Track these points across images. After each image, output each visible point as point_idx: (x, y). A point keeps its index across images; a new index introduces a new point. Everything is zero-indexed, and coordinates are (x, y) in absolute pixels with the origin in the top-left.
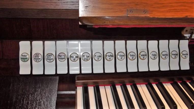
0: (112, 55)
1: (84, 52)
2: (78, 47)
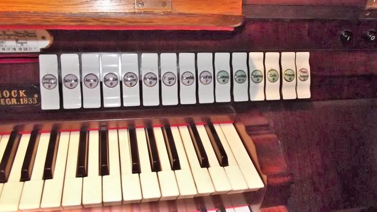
0: (209, 75)
2: (118, 63)
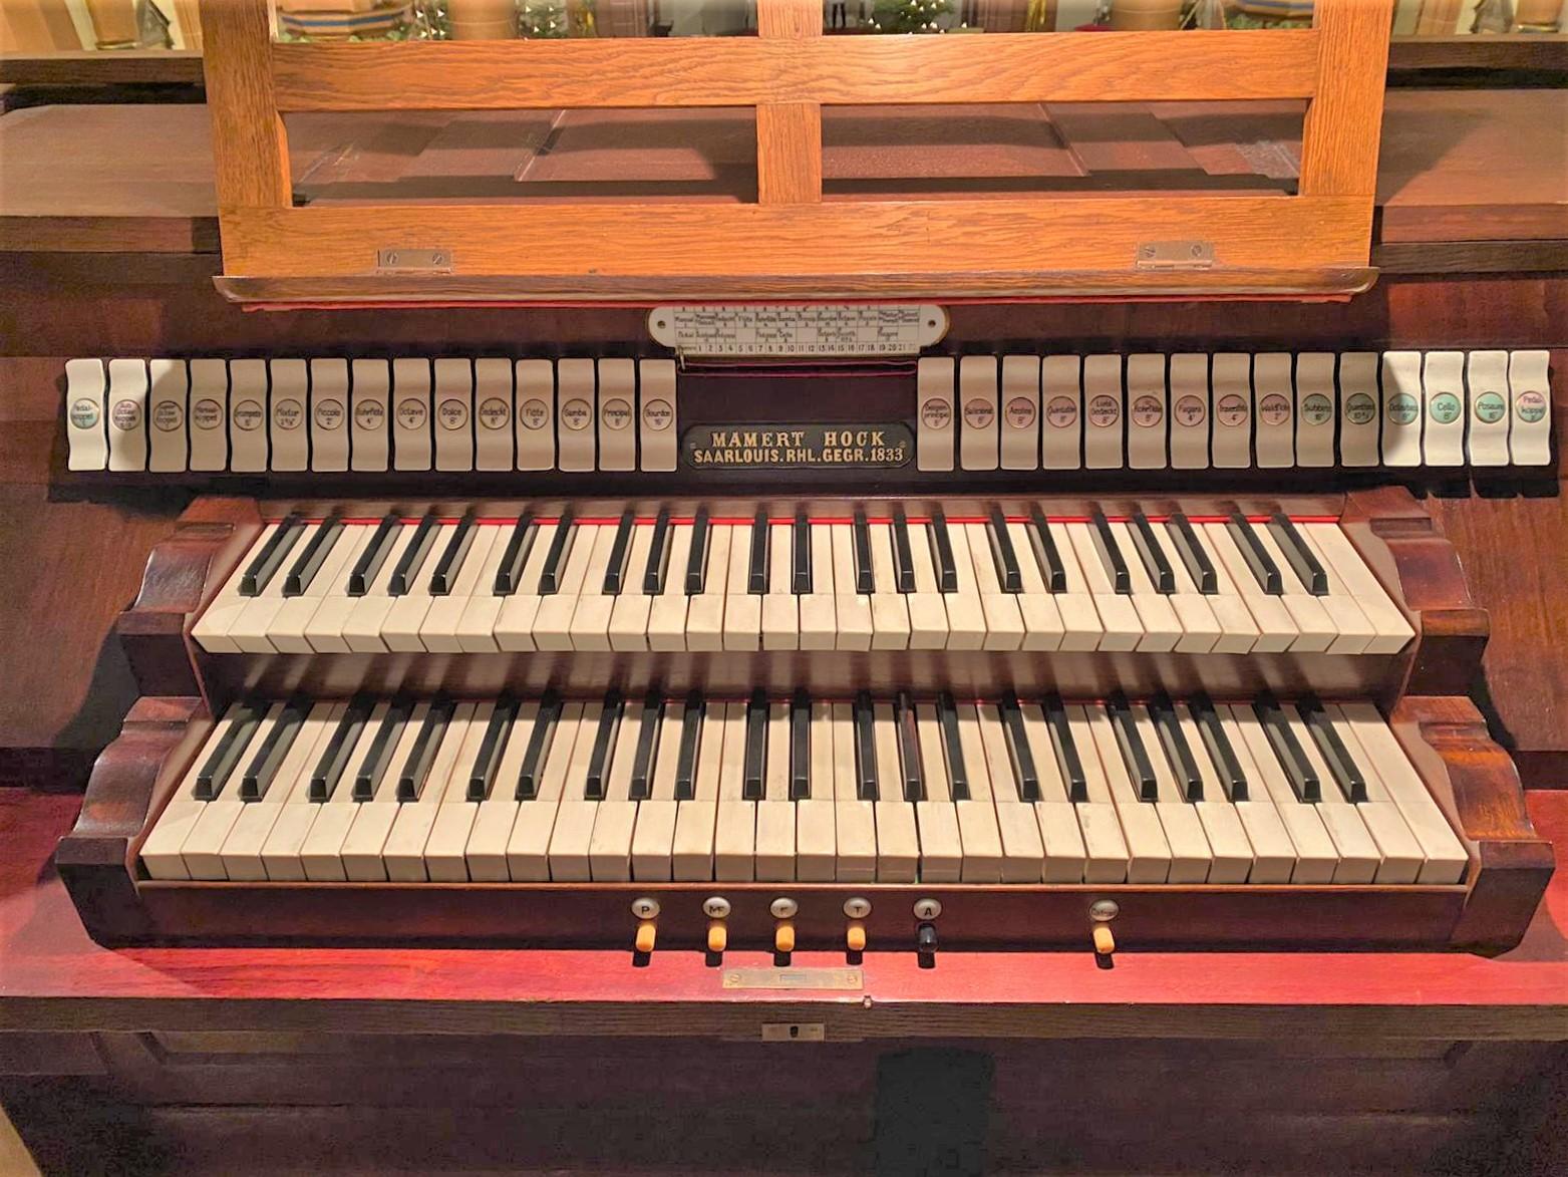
0: (1283, 403)
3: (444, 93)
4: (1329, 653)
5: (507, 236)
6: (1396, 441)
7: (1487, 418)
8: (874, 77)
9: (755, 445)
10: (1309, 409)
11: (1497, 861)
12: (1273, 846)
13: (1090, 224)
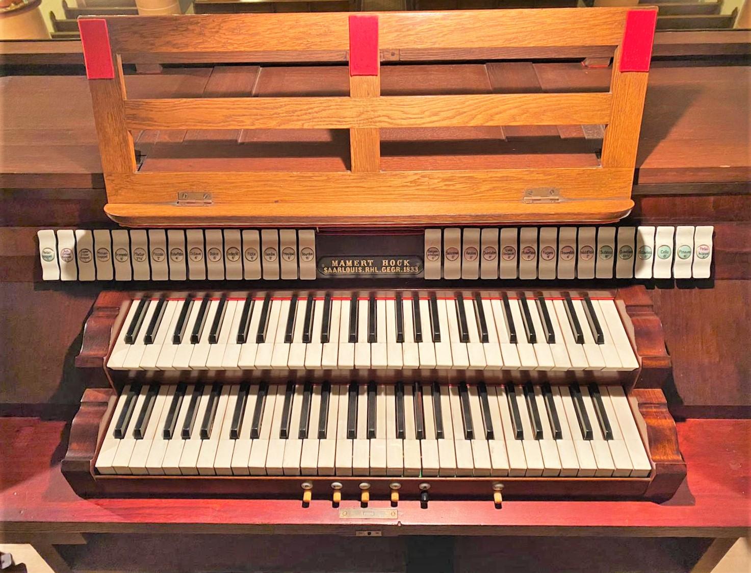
0: (591, 250)
1: (567, 245)
3: (205, 123)
4: (603, 370)
5: (237, 186)
6: (641, 266)
7: (683, 257)
8: (404, 116)
9: (351, 265)
10: (602, 253)
11: (663, 471)
12: (570, 463)
13: (502, 181)
